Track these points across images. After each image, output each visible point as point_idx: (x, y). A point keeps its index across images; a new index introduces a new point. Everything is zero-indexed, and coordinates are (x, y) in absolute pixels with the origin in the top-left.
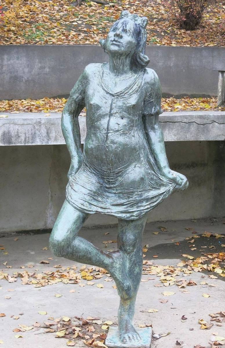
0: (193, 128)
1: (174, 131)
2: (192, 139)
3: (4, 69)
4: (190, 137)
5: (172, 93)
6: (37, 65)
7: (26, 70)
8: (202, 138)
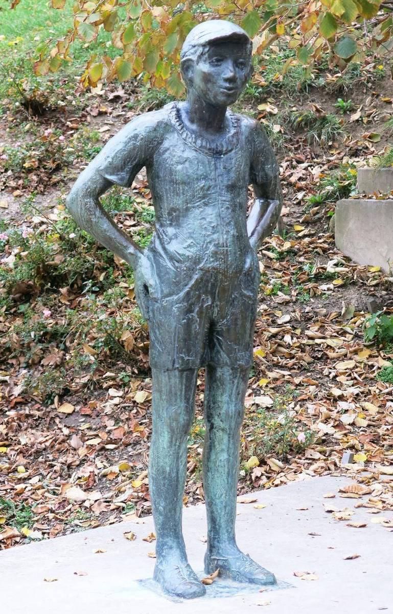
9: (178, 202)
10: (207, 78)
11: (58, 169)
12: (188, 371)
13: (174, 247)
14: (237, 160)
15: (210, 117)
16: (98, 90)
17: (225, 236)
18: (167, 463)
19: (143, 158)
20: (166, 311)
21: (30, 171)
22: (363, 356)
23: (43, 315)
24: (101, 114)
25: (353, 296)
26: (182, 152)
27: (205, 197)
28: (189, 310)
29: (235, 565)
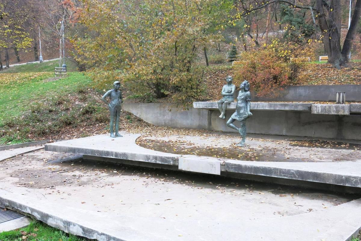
0: (293, 107)
1: (288, 107)
2: (293, 109)
3: (297, 92)
4: (292, 109)
5: (356, 100)
6: (307, 91)
7: (304, 93)
8: (296, 109)
9: (113, 99)
10: (116, 87)
11: (86, 99)
12: (114, 115)
13: (113, 103)
14: (119, 95)
15: (116, 90)
16: (89, 89)
17: (118, 102)
18: (112, 125)
19: (110, 95)
20: (112, 109)
21: (82, 99)
22: (126, 120)
23: (87, 116)
24: (90, 93)
25: (124, 114)
26: (113, 94)
27: (116, 98)
28: (114, 109)
29: (119, 135)
